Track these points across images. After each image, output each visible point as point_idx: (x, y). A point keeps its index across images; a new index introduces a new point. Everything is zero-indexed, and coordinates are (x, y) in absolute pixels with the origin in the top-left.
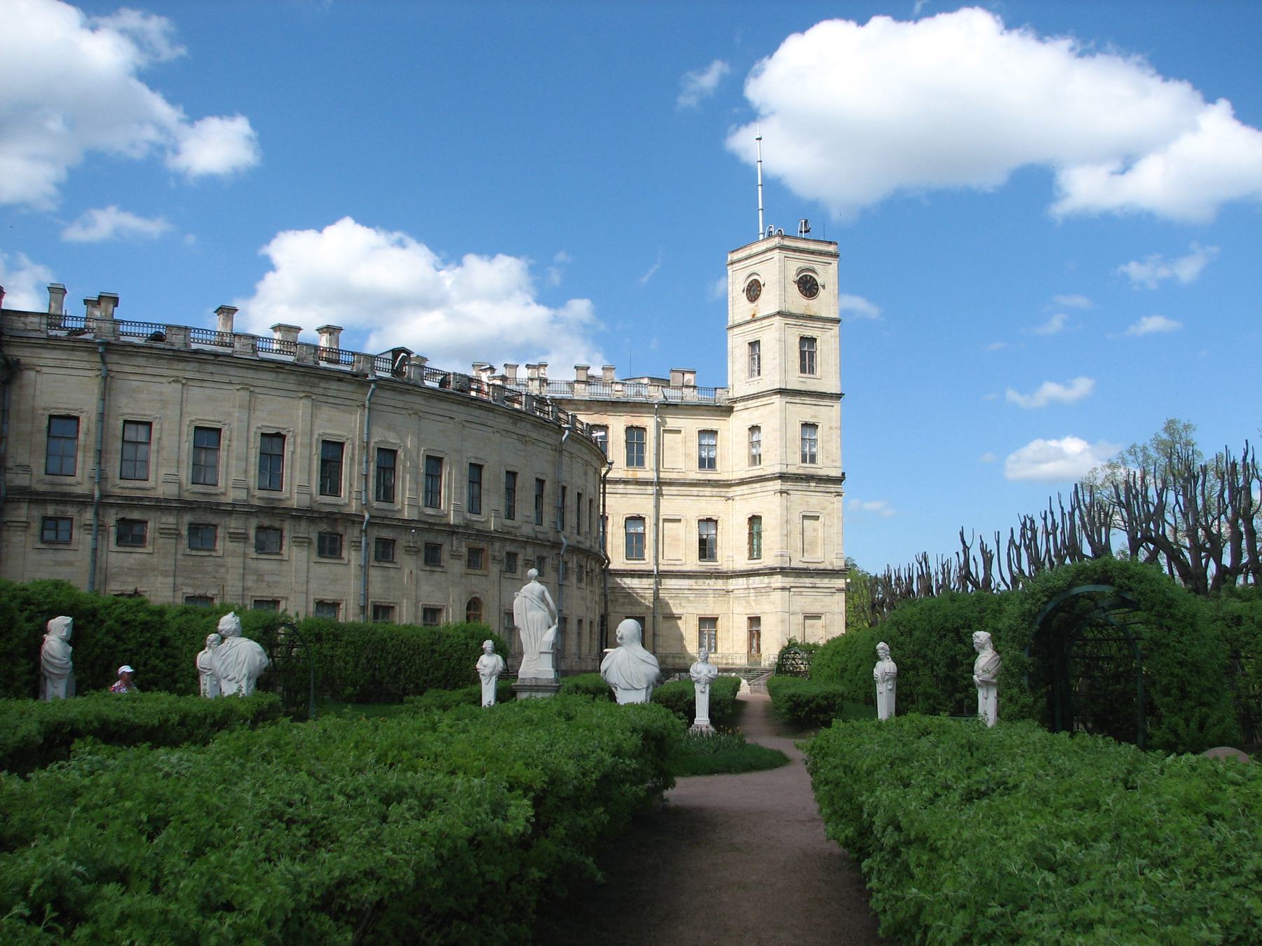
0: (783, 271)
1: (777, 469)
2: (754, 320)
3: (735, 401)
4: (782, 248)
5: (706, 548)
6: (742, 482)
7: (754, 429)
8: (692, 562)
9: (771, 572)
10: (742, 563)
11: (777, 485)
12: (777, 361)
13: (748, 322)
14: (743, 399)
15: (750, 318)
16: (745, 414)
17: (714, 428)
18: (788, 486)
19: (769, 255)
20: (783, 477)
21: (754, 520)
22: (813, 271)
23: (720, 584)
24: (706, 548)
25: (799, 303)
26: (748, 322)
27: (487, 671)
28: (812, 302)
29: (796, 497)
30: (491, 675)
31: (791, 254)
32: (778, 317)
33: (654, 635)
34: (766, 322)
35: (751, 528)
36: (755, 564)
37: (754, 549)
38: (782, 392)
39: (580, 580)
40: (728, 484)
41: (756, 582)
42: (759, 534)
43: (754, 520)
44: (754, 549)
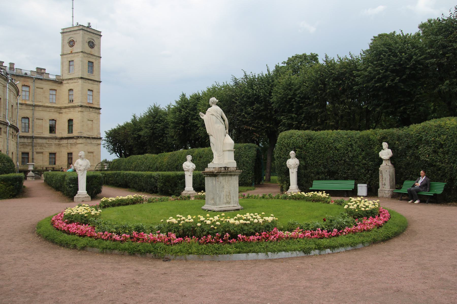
0: (83, 38)
1: (80, 104)
2: (71, 53)
3: (63, 80)
4: (82, 29)
5: (52, 129)
6: (66, 108)
7: (71, 90)
8: (47, 134)
9: (78, 137)
10: (66, 134)
11: (80, 109)
12: (80, 68)
13: (69, 54)
14: (66, 80)
15: (70, 52)
16: (67, 85)
17: (55, 89)
18: (83, 109)
19: (78, 32)
20: (81, 106)
21: (70, 121)
22: (93, 40)
23: (57, 142)
24: (52, 129)
25: (88, 50)
26: (69, 54)
27: (82, 168)
28: (92, 50)
29: (86, 113)
30: (84, 170)
31: (86, 32)
32: (81, 53)
33: (33, 159)
34: (76, 55)
35: (69, 123)
36: (71, 135)
37: (70, 129)
38: (82, 78)
39: (13, 138)
40: (60, 108)
41: (71, 141)
42: (72, 125)
43: (70, 121)
44: (70, 129)
